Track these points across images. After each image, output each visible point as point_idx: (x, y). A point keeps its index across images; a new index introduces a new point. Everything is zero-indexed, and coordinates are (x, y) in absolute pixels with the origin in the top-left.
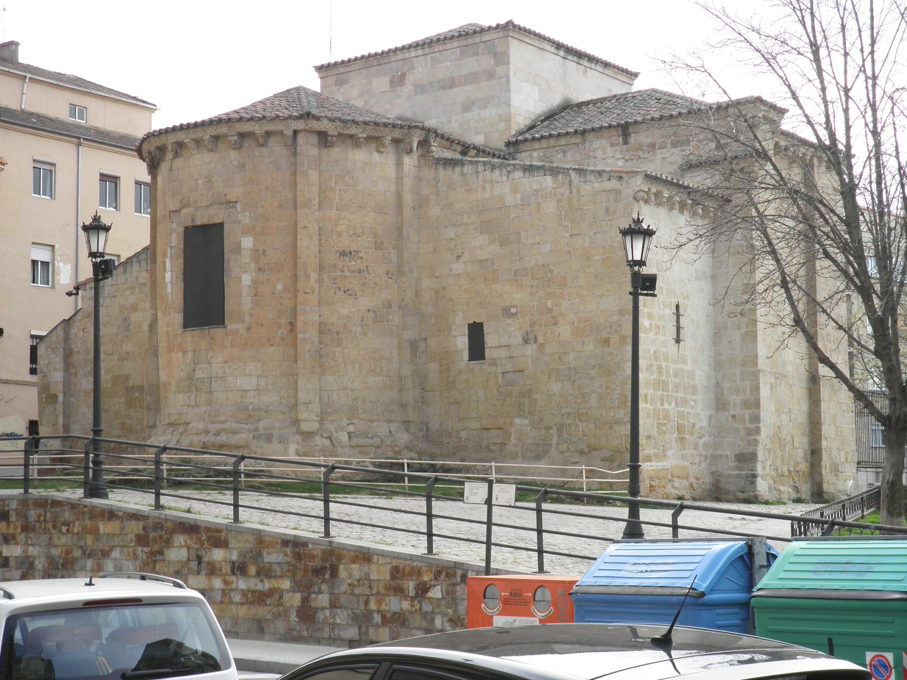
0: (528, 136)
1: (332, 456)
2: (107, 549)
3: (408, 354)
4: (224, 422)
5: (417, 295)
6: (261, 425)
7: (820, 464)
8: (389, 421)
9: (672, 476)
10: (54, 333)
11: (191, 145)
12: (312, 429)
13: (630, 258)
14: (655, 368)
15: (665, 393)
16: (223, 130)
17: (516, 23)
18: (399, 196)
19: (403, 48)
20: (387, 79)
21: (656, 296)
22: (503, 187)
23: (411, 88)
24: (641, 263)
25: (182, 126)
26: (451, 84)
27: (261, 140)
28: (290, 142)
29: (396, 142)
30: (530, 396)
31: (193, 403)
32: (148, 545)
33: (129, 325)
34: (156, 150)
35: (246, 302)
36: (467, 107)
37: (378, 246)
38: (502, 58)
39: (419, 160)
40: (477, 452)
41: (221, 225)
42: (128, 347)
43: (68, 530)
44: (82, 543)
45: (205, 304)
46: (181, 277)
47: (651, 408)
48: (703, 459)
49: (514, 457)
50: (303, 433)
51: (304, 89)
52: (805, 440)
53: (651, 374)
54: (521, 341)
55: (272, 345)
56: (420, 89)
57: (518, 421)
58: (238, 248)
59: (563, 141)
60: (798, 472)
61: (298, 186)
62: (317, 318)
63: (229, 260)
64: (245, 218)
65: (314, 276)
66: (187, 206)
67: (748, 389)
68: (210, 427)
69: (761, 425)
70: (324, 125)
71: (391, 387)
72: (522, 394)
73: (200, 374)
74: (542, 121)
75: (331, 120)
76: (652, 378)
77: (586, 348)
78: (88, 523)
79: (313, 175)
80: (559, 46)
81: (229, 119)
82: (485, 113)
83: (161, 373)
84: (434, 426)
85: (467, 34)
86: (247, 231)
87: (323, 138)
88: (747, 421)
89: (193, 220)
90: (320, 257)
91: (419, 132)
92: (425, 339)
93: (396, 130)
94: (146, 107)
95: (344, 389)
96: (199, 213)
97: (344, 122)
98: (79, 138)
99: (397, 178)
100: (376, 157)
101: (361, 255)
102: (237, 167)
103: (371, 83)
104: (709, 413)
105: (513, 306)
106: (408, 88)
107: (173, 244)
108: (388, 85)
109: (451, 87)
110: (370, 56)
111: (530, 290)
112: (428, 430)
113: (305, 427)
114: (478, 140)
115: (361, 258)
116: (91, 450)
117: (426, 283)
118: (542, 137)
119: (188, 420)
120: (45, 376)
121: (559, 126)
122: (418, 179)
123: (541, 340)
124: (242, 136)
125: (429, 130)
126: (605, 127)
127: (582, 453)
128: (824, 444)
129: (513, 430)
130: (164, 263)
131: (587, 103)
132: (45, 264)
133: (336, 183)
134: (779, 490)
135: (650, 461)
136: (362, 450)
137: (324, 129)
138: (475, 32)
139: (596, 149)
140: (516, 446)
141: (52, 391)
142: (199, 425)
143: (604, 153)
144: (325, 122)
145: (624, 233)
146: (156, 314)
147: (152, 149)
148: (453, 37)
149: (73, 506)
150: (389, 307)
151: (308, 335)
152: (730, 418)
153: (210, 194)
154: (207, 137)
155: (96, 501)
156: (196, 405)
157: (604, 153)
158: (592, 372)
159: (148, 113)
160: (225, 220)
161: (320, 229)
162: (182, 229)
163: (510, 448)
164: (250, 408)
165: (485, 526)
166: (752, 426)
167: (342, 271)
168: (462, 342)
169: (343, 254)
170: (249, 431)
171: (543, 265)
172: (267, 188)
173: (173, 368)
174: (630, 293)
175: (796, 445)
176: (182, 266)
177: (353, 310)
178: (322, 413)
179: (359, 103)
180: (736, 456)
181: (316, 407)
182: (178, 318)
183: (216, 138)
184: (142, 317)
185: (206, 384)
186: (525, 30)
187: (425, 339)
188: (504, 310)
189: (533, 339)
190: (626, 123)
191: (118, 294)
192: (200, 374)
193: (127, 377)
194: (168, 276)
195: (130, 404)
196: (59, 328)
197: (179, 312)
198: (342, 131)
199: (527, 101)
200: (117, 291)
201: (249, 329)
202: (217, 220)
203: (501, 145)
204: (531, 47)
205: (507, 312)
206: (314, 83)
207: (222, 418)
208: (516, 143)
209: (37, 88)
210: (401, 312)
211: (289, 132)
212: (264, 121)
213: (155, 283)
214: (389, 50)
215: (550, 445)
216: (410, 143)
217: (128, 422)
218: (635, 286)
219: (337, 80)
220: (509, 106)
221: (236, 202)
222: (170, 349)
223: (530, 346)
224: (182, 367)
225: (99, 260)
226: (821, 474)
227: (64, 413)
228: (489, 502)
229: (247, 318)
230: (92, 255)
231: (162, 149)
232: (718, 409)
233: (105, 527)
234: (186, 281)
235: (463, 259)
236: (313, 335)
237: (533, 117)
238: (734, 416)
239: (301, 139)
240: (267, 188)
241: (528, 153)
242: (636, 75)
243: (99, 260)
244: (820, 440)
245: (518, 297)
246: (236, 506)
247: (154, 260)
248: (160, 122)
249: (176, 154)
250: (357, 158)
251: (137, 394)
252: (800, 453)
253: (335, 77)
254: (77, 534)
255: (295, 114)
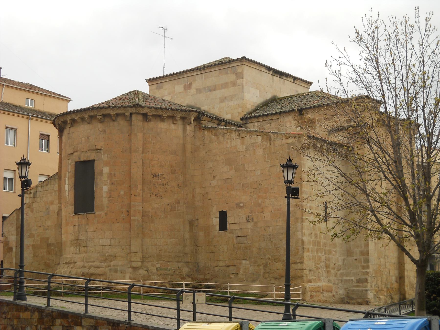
0: (253, 115)
1: (148, 280)
2: (24, 326)
3: (187, 227)
4: (94, 262)
5: (193, 197)
6: (112, 263)
7: (404, 285)
8: (178, 262)
9: (323, 291)
10: (12, 215)
11: (79, 120)
12: (138, 266)
13: (286, 179)
14: (313, 235)
15: (319, 248)
16: (95, 113)
17: (247, 58)
18: (184, 146)
19: (190, 70)
20: (182, 86)
21: (299, 198)
22: (234, 142)
23: (195, 90)
24: (291, 182)
25: (74, 110)
26: (213, 89)
27: (114, 118)
28: (128, 119)
29: (183, 118)
30: (250, 249)
31: (78, 252)
32: (43, 324)
33: (49, 212)
34: (64, 122)
35: (105, 201)
36: (223, 100)
37: (173, 172)
38: (240, 76)
39: (195, 128)
40: (223, 278)
41: (93, 161)
42: (49, 223)
43: (5, 316)
44: (12, 323)
45: (84, 202)
46: (73, 187)
47: (311, 255)
48: (340, 281)
49: (242, 281)
50: (133, 268)
51: (138, 91)
52: (396, 272)
53: (311, 238)
54: (245, 221)
55: (118, 222)
56: (199, 91)
57: (244, 262)
58: (101, 173)
59: (270, 118)
60: (393, 288)
61: (132, 141)
62: (141, 209)
63: (97, 179)
64: (105, 157)
65: (140, 187)
66: (77, 151)
67: (363, 246)
68: (86, 264)
69: (370, 264)
70: (146, 110)
71: (179, 244)
72: (246, 248)
73: (82, 237)
74: (261, 107)
75: (149, 108)
76: (312, 239)
77: (278, 224)
78: (15, 313)
79: (140, 135)
80: (269, 69)
81: (98, 107)
82: (231, 103)
83: (63, 237)
84: (202, 265)
85: (222, 63)
86: (106, 164)
87: (145, 116)
88: (362, 262)
89: (79, 158)
90: (143, 178)
91: (195, 113)
92: (198, 219)
93: (183, 112)
94: (68, 100)
95: (155, 245)
96: (82, 154)
97: (156, 109)
98: (30, 116)
99: (183, 137)
100: (173, 126)
101: (164, 176)
102: (101, 132)
103: (174, 88)
104: (343, 258)
105: (241, 203)
106: (193, 91)
107: (69, 171)
108: (183, 89)
109: (214, 90)
110: (174, 74)
111: (250, 194)
112: (198, 267)
113: (134, 264)
114: (228, 117)
115: (164, 178)
116: (18, 276)
117: (198, 191)
118: (259, 116)
119: (75, 261)
120: (6, 238)
121: (270, 110)
122: (194, 137)
123: (255, 220)
124: (104, 116)
125: (199, 113)
126: (291, 111)
127: (276, 278)
128: (406, 273)
129: (241, 267)
130: (65, 180)
131: (284, 98)
132: (11, 180)
133: (152, 140)
134: (379, 298)
135: (311, 283)
136: (164, 276)
137: (145, 112)
138: (226, 62)
139: (286, 122)
140: (242, 275)
141: (10, 246)
142: (80, 264)
143: (291, 124)
144: (146, 109)
145: (283, 167)
146: (61, 206)
147: (60, 122)
148: (215, 65)
149: (8, 304)
150: (179, 203)
151: (136, 218)
152: (354, 260)
153: (88, 145)
154: (86, 116)
155: (19, 302)
156: (80, 253)
157: (291, 124)
158: (281, 237)
159: (66, 102)
160: (95, 159)
161: (143, 163)
162: (74, 163)
163: (240, 276)
164: (107, 255)
165: (233, 316)
166: (365, 264)
167: (154, 185)
168: (216, 221)
169: (155, 176)
170: (106, 267)
171: (257, 182)
172: (116, 142)
173: (68, 234)
174: (286, 197)
175: (391, 274)
176: (74, 182)
177: (160, 204)
178: (143, 257)
179: (168, 98)
180: (357, 280)
181: (140, 254)
182: (71, 208)
183: (91, 117)
184: (54, 208)
185: (84, 242)
186: (251, 61)
187: (198, 219)
188: (237, 204)
189: (251, 220)
190: (301, 108)
191: (44, 196)
192: (82, 237)
193: (48, 238)
194: (67, 187)
195: (49, 252)
196: (14, 213)
197: (72, 206)
198: (154, 113)
199: (253, 97)
200: (44, 194)
201: (106, 214)
202: (92, 158)
203: (238, 120)
204: (255, 70)
205: (238, 206)
206: (145, 89)
207: (92, 260)
208: (247, 118)
209: (9, 90)
210: (185, 205)
211: (127, 114)
212: (115, 108)
213: (60, 190)
214: (183, 71)
215: (260, 274)
216: (190, 119)
217: (48, 261)
218: (288, 194)
219: (157, 87)
220: (243, 99)
221: (101, 149)
222: (67, 224)
223: (249, 223)
224: (73, 234)
225: (23, 179)
226: (404, 290)
227: (16, 257)
228: (194, 303)
229: (106, 209)
230: (21, 177)
231: (65, 122)
232: (348, 256)
233: (23, 315)
234: (75, 189)
235: (217, 178)
236: (139, 217)
237: (256, 105)
238: (356, 259)
239: (134, 117)
240: (116, 142)
241: (252, 124)
242: (311, 83)
243: (23, 179)
244: (404, 271)
245: (244, 198)
246: (86, 305)
247: (60, 179)
248: (71, 107)
249: (72, 125)
250: (162, 127)
251: (52, 248)
252: (394, 278)
253: (156, 85)
254: (10, 318)
255: (131, 105)
